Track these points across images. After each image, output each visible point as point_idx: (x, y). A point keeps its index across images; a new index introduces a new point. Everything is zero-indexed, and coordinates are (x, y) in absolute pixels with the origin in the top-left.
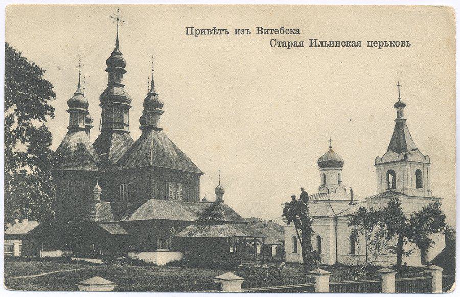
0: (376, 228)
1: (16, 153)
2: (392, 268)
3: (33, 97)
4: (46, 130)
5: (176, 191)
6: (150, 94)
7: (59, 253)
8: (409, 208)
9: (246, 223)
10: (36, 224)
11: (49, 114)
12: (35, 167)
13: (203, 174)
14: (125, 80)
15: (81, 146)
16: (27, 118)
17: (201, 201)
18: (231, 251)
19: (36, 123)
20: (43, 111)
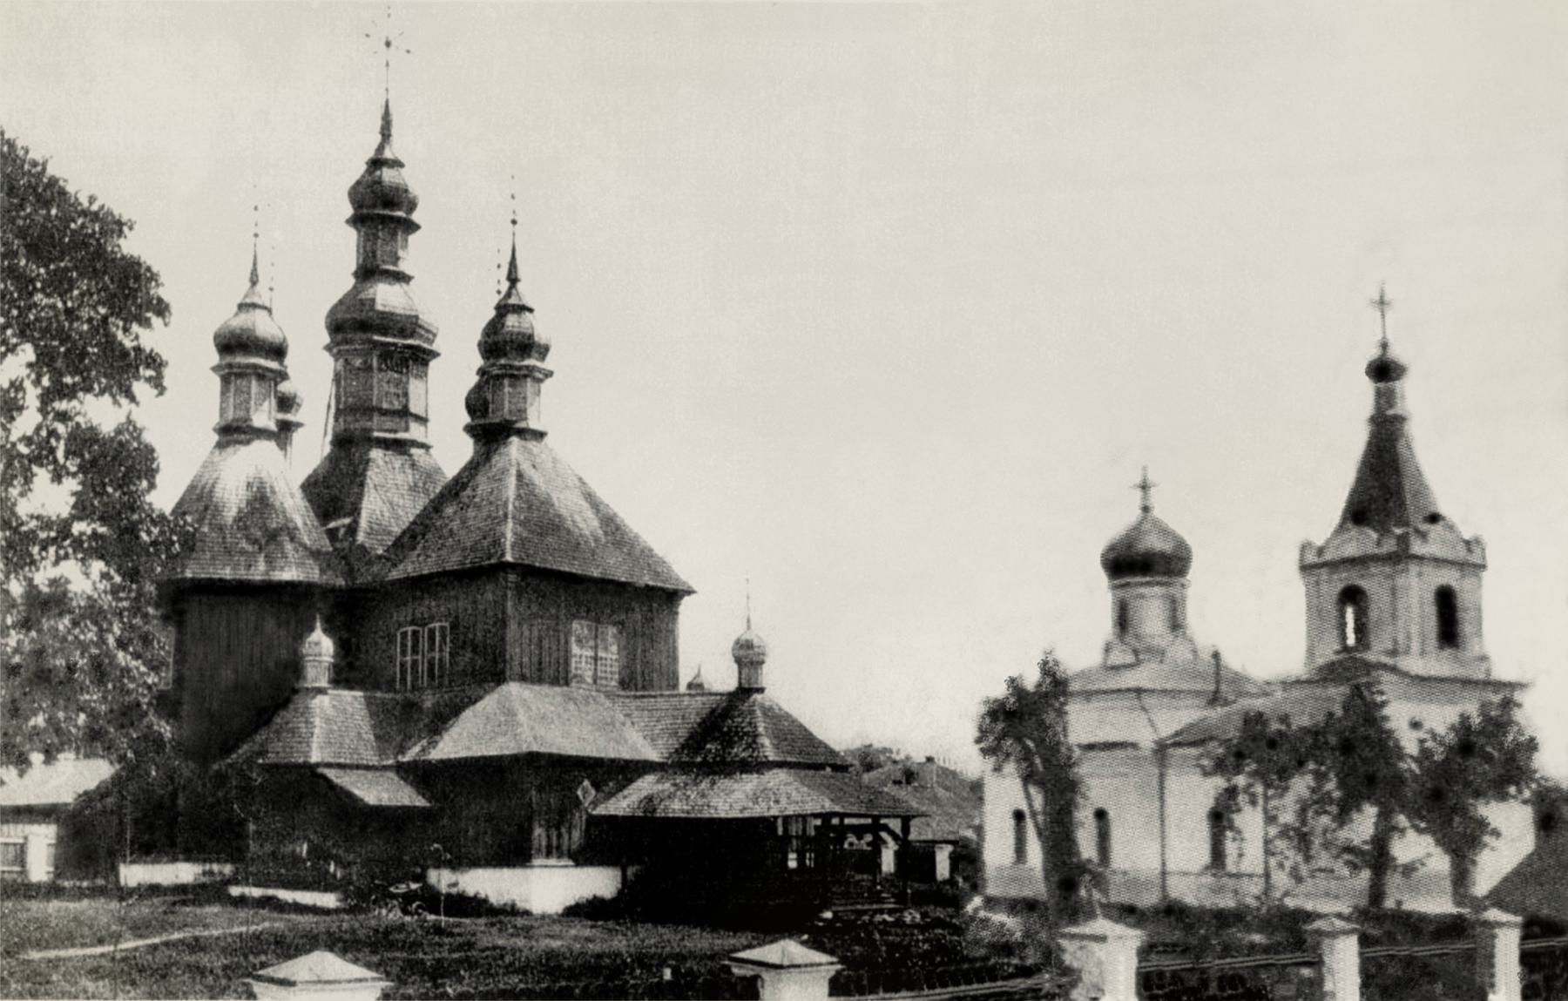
0: (1301, 785)
1: (32, 517)
2: (1347, 919)
3: (90, 320)
4: (138, 439)
5: (594, 651)
6: (503, 309)
7: (185, 872)
8: (1417, 722)
9: (841, 769)
10: (99, 771)
11: (149, 380)
12: (98, 566)
13: (690, 592)
14: (413, 254)
15: (260, 500)
16: (70, 393)
17: (682, 688)
18: (792, 864)
19: (99, 412)
20: (123, 368)
